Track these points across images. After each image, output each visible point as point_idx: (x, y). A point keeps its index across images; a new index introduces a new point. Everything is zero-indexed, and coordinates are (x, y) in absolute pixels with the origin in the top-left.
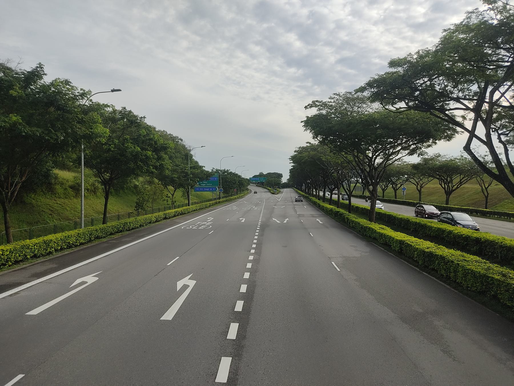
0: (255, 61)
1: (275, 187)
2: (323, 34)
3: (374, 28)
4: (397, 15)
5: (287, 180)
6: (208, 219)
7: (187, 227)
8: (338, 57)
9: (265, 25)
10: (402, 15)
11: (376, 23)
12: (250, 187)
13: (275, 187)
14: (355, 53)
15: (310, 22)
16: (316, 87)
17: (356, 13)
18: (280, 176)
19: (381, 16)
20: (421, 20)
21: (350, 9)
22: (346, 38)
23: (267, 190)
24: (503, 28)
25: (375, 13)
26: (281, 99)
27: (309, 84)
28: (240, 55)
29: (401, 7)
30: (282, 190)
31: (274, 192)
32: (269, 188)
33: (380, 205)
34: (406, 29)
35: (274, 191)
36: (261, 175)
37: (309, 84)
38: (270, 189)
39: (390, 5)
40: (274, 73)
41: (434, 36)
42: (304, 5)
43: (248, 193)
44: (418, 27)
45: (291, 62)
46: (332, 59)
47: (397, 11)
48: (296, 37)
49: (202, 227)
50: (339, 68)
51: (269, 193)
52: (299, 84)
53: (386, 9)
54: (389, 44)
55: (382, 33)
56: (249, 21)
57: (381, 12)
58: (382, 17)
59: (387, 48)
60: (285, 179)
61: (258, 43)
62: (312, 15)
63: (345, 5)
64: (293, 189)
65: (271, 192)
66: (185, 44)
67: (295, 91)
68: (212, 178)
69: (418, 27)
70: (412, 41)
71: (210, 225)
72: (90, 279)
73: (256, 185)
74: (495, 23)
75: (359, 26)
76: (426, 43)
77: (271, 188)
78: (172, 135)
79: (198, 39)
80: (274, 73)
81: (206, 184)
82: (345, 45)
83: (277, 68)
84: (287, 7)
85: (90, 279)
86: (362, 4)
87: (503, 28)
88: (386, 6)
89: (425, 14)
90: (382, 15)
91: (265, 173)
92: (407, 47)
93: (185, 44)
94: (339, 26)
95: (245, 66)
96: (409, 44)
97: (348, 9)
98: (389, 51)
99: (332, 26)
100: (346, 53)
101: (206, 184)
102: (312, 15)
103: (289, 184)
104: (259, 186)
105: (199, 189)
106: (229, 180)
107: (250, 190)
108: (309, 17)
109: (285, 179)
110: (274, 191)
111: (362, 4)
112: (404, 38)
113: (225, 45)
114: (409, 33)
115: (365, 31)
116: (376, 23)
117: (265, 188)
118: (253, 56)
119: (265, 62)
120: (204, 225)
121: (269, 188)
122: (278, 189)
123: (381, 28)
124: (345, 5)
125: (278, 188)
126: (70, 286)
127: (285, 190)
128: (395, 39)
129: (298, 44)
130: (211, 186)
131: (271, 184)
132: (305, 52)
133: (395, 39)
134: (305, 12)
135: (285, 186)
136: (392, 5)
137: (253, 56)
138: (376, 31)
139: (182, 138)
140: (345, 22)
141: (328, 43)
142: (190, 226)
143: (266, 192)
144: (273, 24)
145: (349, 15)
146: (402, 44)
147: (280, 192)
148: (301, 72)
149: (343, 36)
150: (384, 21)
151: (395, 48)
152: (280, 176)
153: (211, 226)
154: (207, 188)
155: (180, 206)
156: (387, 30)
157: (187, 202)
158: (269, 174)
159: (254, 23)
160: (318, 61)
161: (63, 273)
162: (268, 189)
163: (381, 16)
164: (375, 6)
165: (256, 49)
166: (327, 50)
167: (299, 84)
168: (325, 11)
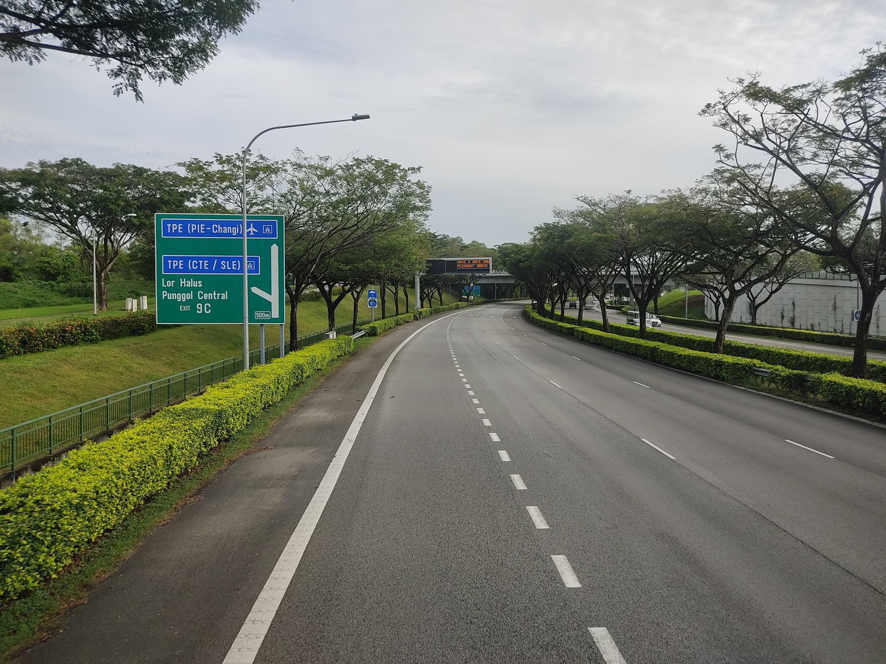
81: (195, 295)
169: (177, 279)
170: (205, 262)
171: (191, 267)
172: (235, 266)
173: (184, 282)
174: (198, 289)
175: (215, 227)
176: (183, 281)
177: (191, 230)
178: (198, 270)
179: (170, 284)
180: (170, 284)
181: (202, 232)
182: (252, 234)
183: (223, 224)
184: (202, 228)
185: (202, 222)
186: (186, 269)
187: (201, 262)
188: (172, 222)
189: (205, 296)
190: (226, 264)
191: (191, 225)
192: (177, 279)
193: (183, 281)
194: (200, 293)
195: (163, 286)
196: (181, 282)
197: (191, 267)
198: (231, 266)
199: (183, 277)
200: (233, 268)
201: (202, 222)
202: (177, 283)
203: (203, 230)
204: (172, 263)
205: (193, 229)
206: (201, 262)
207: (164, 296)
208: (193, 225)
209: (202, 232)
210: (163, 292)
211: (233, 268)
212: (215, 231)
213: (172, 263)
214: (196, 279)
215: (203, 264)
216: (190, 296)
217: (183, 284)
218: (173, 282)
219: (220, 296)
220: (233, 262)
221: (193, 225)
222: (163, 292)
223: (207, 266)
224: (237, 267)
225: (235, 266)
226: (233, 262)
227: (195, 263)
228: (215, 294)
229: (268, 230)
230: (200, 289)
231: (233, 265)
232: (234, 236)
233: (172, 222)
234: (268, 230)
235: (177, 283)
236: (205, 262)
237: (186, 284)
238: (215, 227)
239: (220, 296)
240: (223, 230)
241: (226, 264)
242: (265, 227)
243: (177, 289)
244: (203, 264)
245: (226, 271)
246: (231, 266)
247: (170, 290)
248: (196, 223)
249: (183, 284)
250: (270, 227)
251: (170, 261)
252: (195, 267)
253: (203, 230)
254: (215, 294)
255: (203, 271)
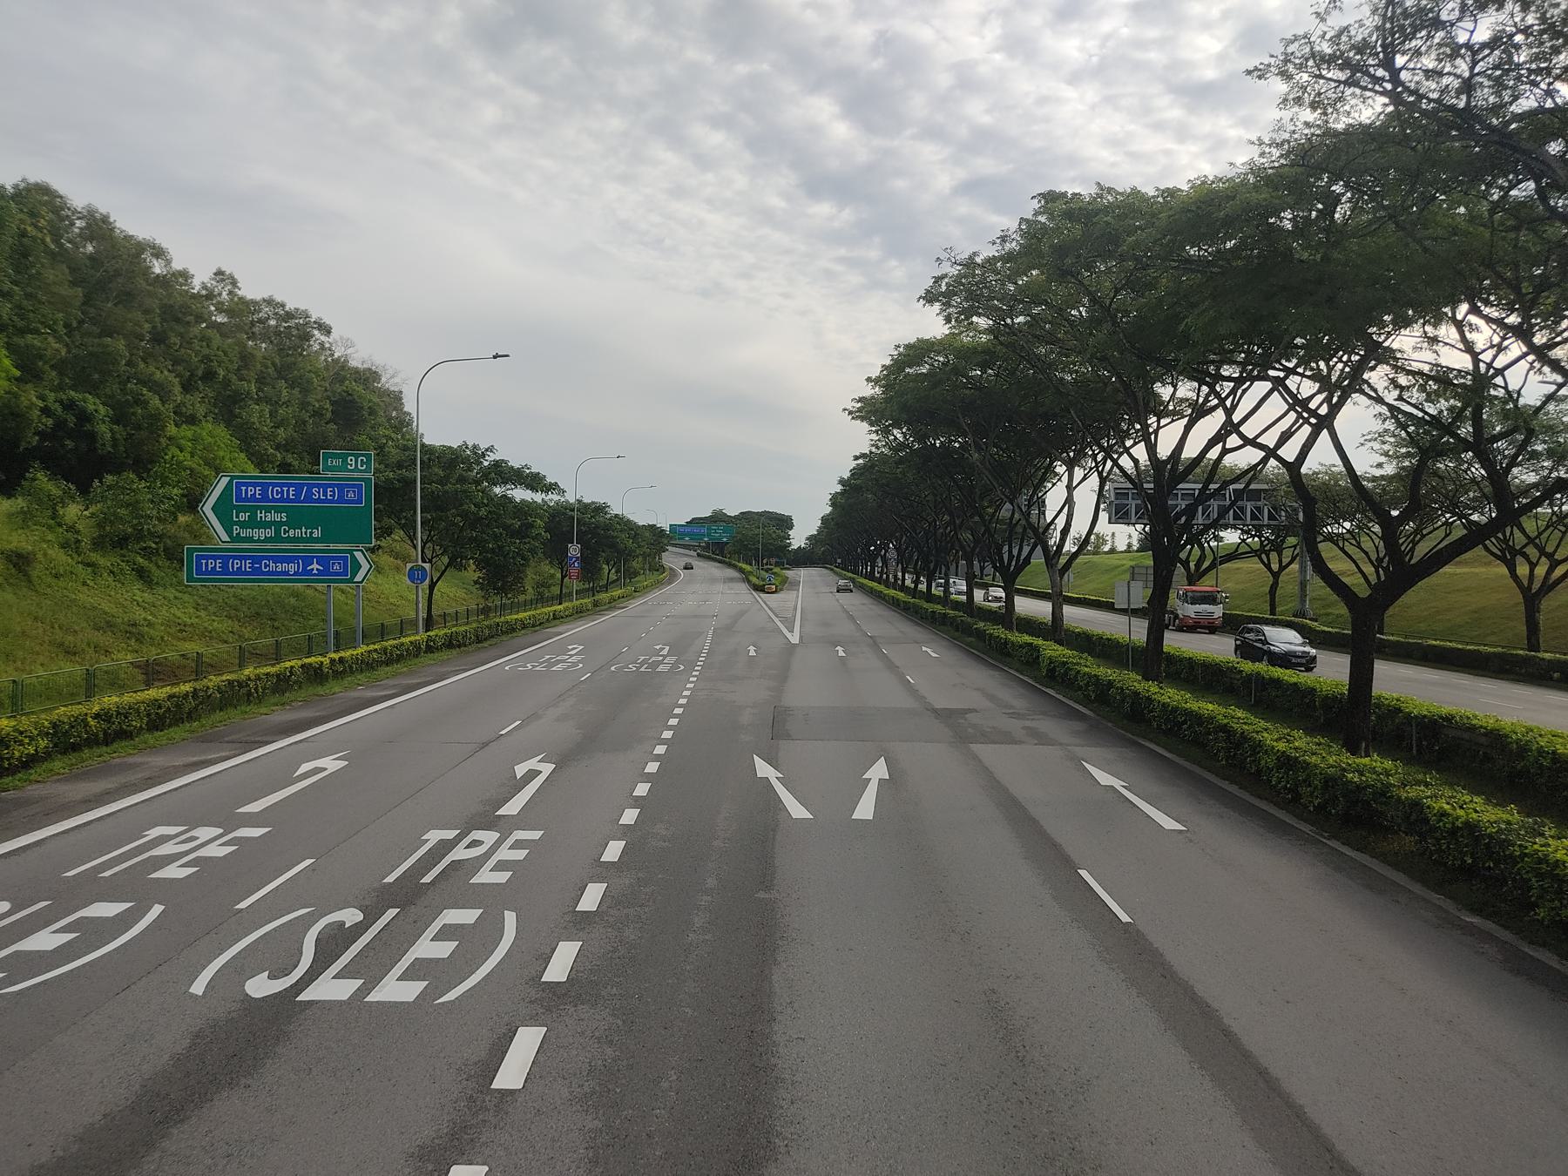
0: (710, 177)
1: (765, 561)
2: (918, 105)
3: (1070, 93)
4: (1139, 55)
5: (807, 539)
6: (570, 647)
7: (520, 666)
8: (962, 174)
9: (742, 69)
10: (1153, 56)
11: (1075, 78)
12: (672, 558)
13: (765, 561)
14: (1011, 166)
15: (877, 64)
16: (893, 263)
17: (1018, 45)
18: (785, 523)
19: (1091, 56)
20: (1210, 74)
21: (998, 31)
22: (986, 119)
23: (735, 574)
24: (1229, 245)
25: (1072, 46)
26: (786, 296)
27: (874, 254)
28: (667, 158)
29: (1153, 33)
30: (790, 574)
31: (762, 583)
32: (744, 566)
33: (1175, 642)
34: (1165, 100)
35: (764, 580)
36: (718, 518)
37: (874, 254)
38: (747, 567)
39: (1116, 24)
40: (766, 216)
41: (1246, 122)
42: (860, 14)
43: (659, 584)
44: (1199, 95)
45: (819, 184)
46: (944, 181)
47: (1140, 44)
48: (836, 109)
49: (559, 666)
50: (964, 207)
51: (743, 588)
52: (843, 252)
53: (1107, 38)
54: (1113, 142)
55: (1093, 107)
56: (692, 54)
57: (1092, 44)
58: (1095, 59)
59: (1105, 154)
60: (798, 538)
61: (718, 122)
62: (885, 43)
63: (984, 20)
64: (832, 570)
65: (749, 582)
66: (490, 113)
67: (829, 275)
68: (325, 487)
69: (1199, 95)
70: (1182, 133)
71: (579, 662)
72: (331, 764)
73: (699, 555)
74: (1535, 16)
75: (1025, 85)
76: (1218, 144)
77: (751, 565)
78: (283, 306)
79: (531, 99)
80: (766, 216)
81: (277, 532)
82: (983, 140)
83: (776, 202)
84: (810, 16)
85: (331, 764)
86: (1035, 20)
87: (1229, 245)
88: (1106, 26)
89: (1221, 58)
90: (1093, 56)
91: (732, 511)
92: (1167, 153)
93: (490, 113)
94: (967, 80)
95: (678, 192)
96: (1171, 145)
97: (993, 31)
98: (1113, 165)
99: (944, 80)
100: (986, 165)
101: (277, 532)
102: (885, 43)
103: (813, 553)
104: (709, 558)
105: (225, 566)
106: (483, 512)
107: (671, 569)
108: (875, 50)
109: (798, 538)
110: (764, 580)
111: (1035, 20)
112: (1159, 127)
113: (616, 123)
114: (1174, 113)
115: (1043, 100)
116: (1076, 78)
117: (730, 565)
118: (703, 161)
119: (741, 181)
120: (564, 661)
121: (744, 566)
122: (777, 570)
123: (1091, 92)
124: (984, 20)
125: (777, 564)
126: (295, 773)
127: (802, 574)
128: (1132, 127)
129: (842, 131)
130: (317, 540)
131: (750, 550)
132: (862, 156)
133: (1132, 127)
134: (863, 33)
135: (803, 559)
136: (1126, 26)
137: (703, 161)
138: (1075, 101)
139: (327, 320)
140: (983, 70)
141: (933, 133)
142: (528, 665)
143: (731, 580)
144: (765, 67)
145: (997, 49)
146: (1152, 143)
147: (785, 580)
148: (847, 215)
149: (977, 111)
150: (1101, 70)
151: (1135, 156)
152: (785, 523)
153: (581, 665)
154: (289, 560)
155: (237, 661)
156: (1109, 100)
157: (559, 593)
158: (746, 516)
159: (709, 59)
160: (900, 184)
161: (159, 795)
162: (741, 570)
163: (1091, 56)
164: (1075, 26)
165: (715, 139)
166: (929, 152)
167: (843, 252)
168: (925, 34)
169: (253, 511)
170: (291, 489)
171: (273, 495)
172: (330, 496)
173: (263, 515)
174: (281, 523)
175: (265, 563)
176: (261, 513)
177: (233, 569)
178: (281, 500)
179: (243, 517)
180: (243, 517)
181: (248, 570)
182: (315, 572)
183: (276, 560)
184: (248, 565)
185: (245, 558)
186: (265, 498)
187: (285, 489)
188: (207, 558)
189: (291, 533)
190: (319, 493)
191: (233, 562)
192: (253, 511)
193: (261, 513)
194: (285, 529)
195: (235, 519)
196: (259, 515)
197: (273, 495)
198: (325, 494)
199: (261, 508)
200: (329, 497)
201: (245, 558)
202: (253, 517)
203: (249, 568)
204: (246, 490)
205: (236, 566)
206: (285, 489)
207: (235, 532)
208: (236, 561)
209: (248, 570)
210: (235, 527)
211: (329, 497)
212: (265, 568)
213: (246, 490)
214: (278, 510)
215: (288, 491)
216: (270, 533)
217: (261, 517)
218: (247, 514)
219: (311, 533)
220: (329, 490)
221: (236, 561)
222: (235, 527)
223: (293, 495)
224: (333, 496)
225: (330, 496)
226: (329, 490)
227: (277, 490)
228: (304, 530)
229: (336, 567)
230: (284, 524)
231: (329, 493)
232: (291, 575)
233: (207, 558)
234: (336, 567)
235: (253, 517)
236: (291, 489)
237: (265, 517)
238: (265, 563)
239: (311, 533)
240: (276, 567)
241: (319, 493)
242: (334, 564)
243: (253, 523)
244: (288, 491)
245: (319, 500)
246: (325, 494)
247: (243, 525)
248: (241, 558)
249: (261, 517)
250: (354, 492)
251: (244, 488)
252: (277, 495)
253: (249, 568)
254: (304, 530)
255: (288, 500)
